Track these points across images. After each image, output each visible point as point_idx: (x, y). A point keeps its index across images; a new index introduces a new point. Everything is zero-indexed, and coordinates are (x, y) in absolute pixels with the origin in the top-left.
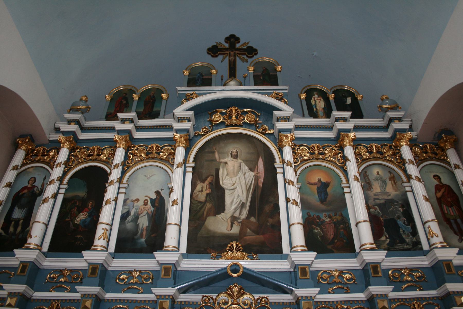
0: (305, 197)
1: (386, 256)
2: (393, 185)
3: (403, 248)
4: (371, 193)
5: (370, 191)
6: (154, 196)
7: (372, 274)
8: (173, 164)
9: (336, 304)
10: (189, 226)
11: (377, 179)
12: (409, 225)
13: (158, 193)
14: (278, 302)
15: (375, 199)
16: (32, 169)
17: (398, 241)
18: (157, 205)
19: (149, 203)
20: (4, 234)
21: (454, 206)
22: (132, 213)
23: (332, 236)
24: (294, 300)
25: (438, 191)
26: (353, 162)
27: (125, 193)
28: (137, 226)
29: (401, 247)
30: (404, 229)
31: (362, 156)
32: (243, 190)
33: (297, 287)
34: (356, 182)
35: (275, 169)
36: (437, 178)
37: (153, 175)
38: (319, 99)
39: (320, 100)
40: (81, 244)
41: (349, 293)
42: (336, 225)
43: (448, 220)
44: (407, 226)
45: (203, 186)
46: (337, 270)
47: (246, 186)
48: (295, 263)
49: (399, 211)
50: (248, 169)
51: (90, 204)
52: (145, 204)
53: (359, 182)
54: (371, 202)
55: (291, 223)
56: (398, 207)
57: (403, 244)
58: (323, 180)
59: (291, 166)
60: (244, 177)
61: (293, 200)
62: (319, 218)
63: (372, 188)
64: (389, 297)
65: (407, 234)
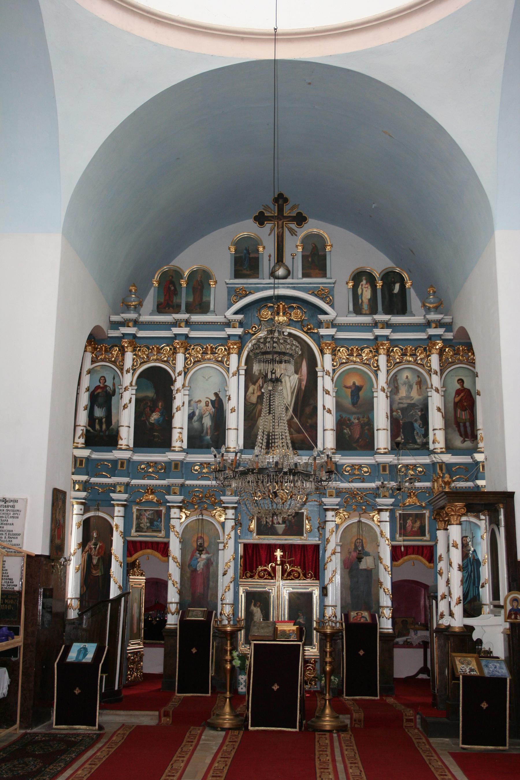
0: (340, 400)
2: (418, 390)
4: (397, 398)
6: (213, 398)
11: (405, 383)
13: (216, 394)
15: (399, 403)
18: (217, 406)
19: (210, 404)
20: (92, 431)
22: (197, 413)
23: (358, 436)
27: (189, 395)
28: (202, 425)
30: (418, 431)
35: (316, 372)
37: (210, 377)
38: (367, 286)
39: (368, 287)
40: (159, 440)
42: (363, 426)
43: (458, 424)
45: (254, 388)
47: (291, 389)
49: (418, 414)
52: (207, 405)
54: (395, 407)
55: (325, 428)
62: (349, 420)
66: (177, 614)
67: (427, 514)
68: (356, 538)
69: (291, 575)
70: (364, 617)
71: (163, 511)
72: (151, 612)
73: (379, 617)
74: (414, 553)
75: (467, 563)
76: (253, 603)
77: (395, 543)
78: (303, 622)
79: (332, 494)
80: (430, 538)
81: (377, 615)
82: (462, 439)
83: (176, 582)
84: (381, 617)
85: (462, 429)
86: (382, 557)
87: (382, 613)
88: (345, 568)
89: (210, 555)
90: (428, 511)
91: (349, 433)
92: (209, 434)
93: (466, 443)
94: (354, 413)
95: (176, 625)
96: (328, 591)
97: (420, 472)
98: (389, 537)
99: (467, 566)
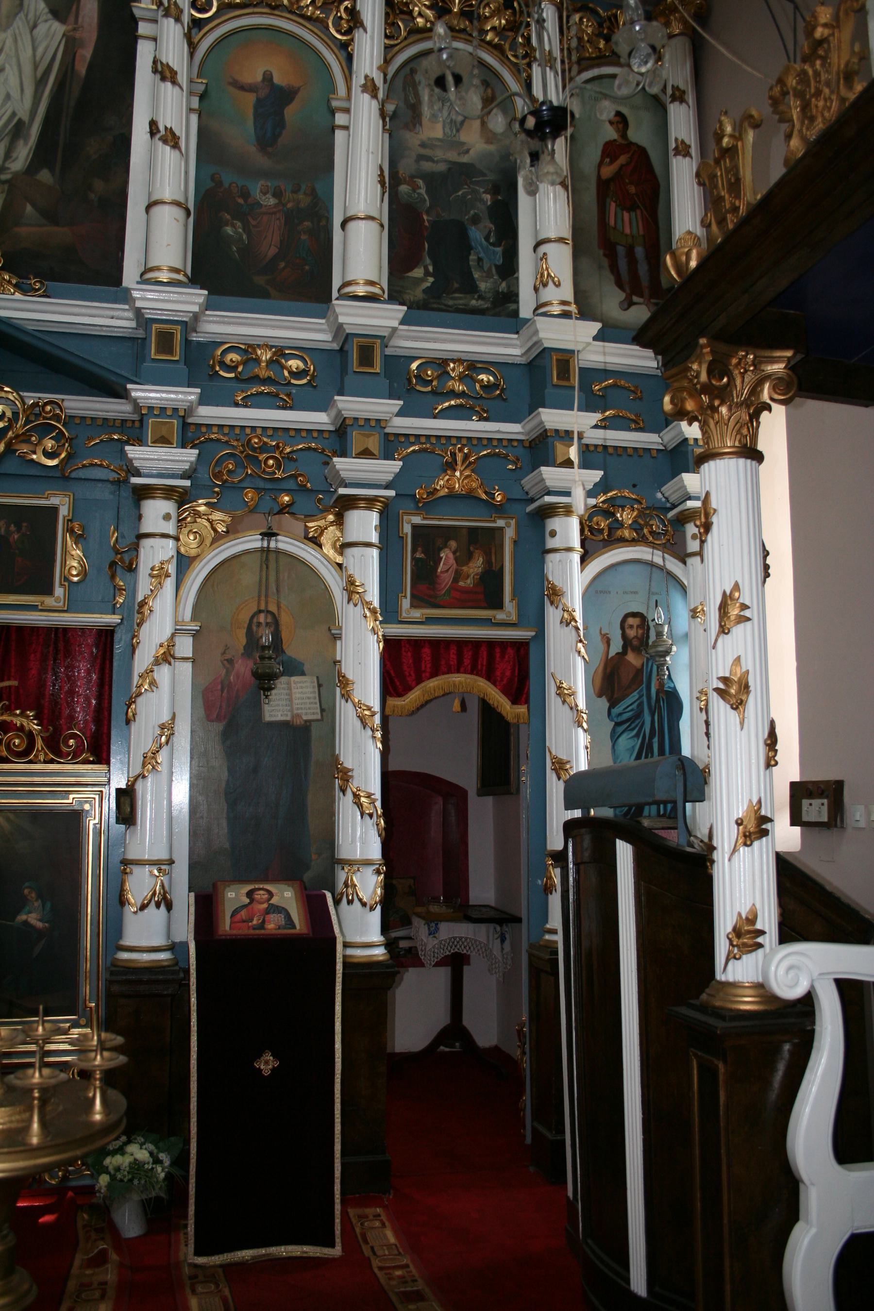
1: (402, 323)
3: (465, 305)
4: (413, 139)
5: (410, 131)
9: (248, 435)
12: (500, 246)
14: (92, 418)
15: (421, 158)
17: (456, 285)
21: (638, 207)
23: (273, 251)
24: (136, 416)
25: (607, 160)
26: (373, 33)
29: (461, 302)
30: (482, 255)
31: (414, 19)
32: (24, 79)
33: (138, 380)
34: (367, 97)
35: (134, 22)
36: (617, 122)
41: (291, 408)
43: (609, 247)
44: (491, 248)
46: (267, 346)
47: (36, 67)
48: (344, 330)
49: (481, 200)
50: (47, 10)
53: (377, 99)
54: (407, 166)
56: (482, 190)
57: (468, 296)
59: (178, 20)
60: (29, 36)
61: (166, 128)
62: (245, 194)
63: (421, 124)
64: (584, 439)
65: (486, 269)
67: (510, 534)
68: (255, 609)
70: (278, 909)
73: (337, 902)
74: (462, 669)
75: (641, 705)
77: (396, 630)
78: (40, 925)
79: (164, 432)
80: (519, 616)
81: (329, 895)
82: (623, 296)
84: (345, 900)
85: (623, 264)
86: (350, 676)
87: (346, 885)
88: (209, 718)
90: (513, 522)
91: (241, 239)
93: (633, 308)
94: (266, 174)
96: (139, 803)
97: (486, 387)
98: (376, 604)
99: (638, 715)
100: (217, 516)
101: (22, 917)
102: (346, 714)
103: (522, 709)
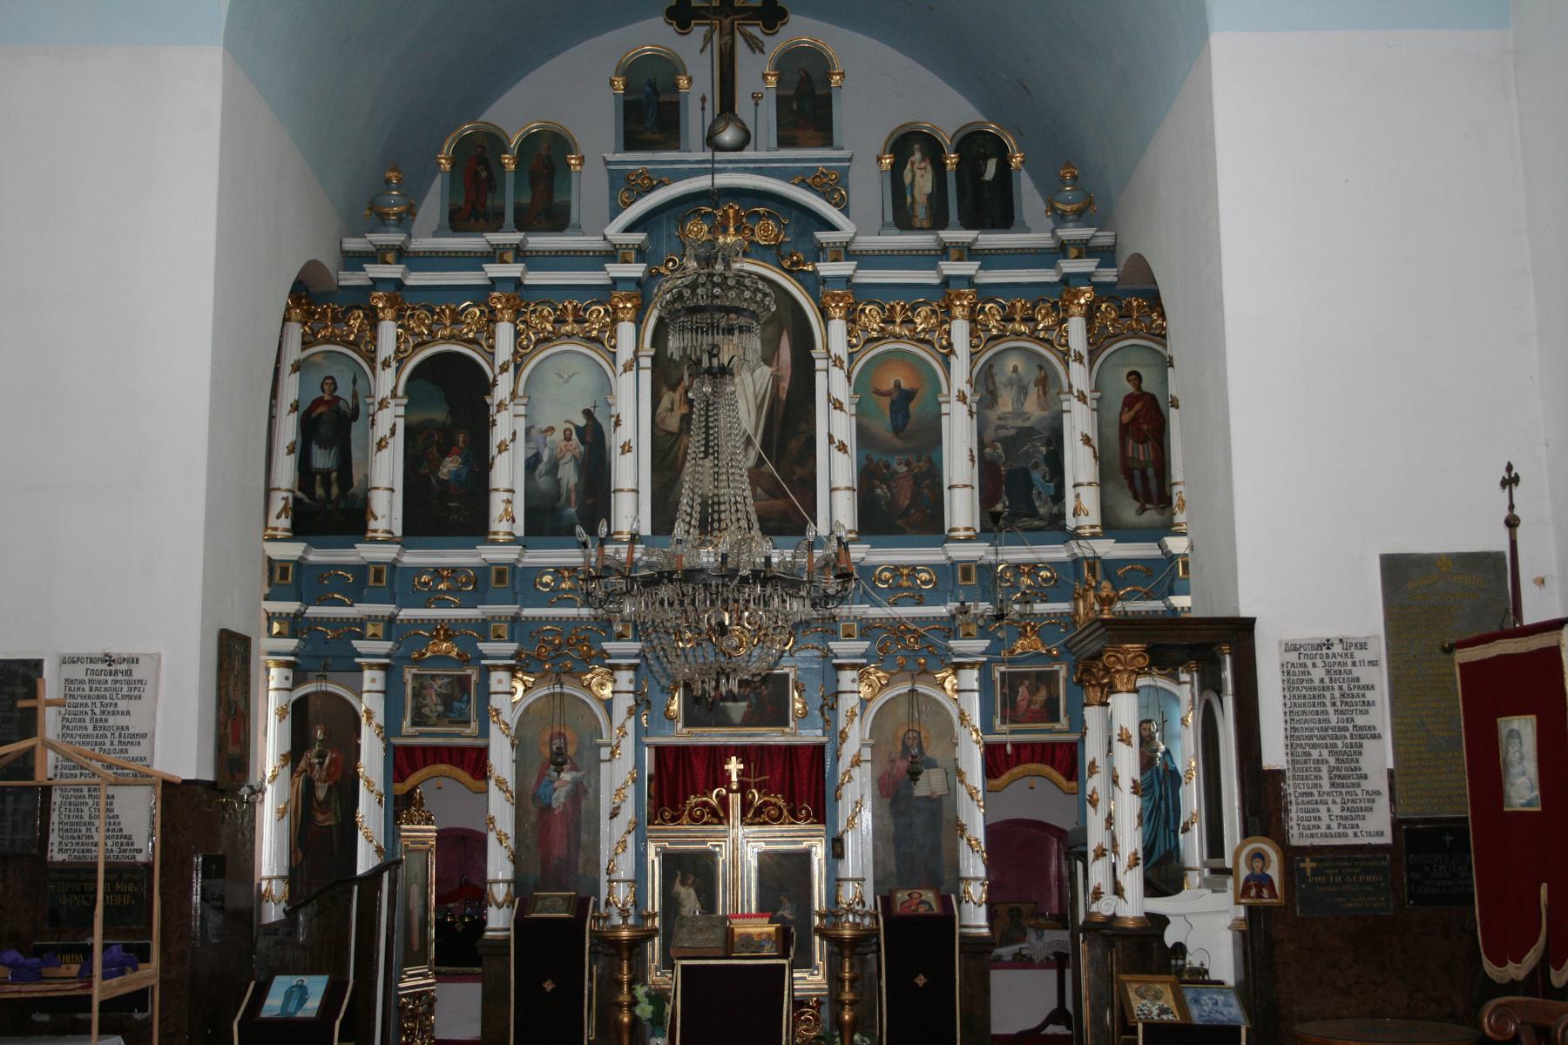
2: (1039, 396)
4: (992, 415)
6: (582, 422)
7: (960, 579)
8: (612, 350)
10: (653, 483)
11: (1010, 383)
13: (588, 414)
15: (999, 427)
16: (321, 355)
19: (574, 436)
20: (307, 500)
22: (545, 457)
23: (907, 503)
27: (526, 416)
28: (558, 482)
30: (1041, 490)
35: (813, 361)
37: (575, 374)
38: (923, 165)
39: (925, 168)
40: (461, 520)
42: (917, 479)
43: (1128, 472)
47: (756, 398)
51: (461, 439)
52: (568, 438)
54: (990, 434)
55: (833, 486)
58: (904, 385)
62: (888, 466)
66: (508, 907)
67: (1063, 673)
69: (763, 813)
71: (474, 678)
72: (452, 905)
73: (959, 902)
75: (1152, 780)
76: (678, 878)
78: (790, 917)
82: (1138, 505)
83: (505, 835)
86: (964, 770)
89: (580, 774)
92: (573, 504)
95: (508, 930)
96: (846, 846)
97: (1046, 580)
98: (978, 726)
100: (880, 674)
101: (780, 913)
102: (962, 792)
103: (1074, 784)
